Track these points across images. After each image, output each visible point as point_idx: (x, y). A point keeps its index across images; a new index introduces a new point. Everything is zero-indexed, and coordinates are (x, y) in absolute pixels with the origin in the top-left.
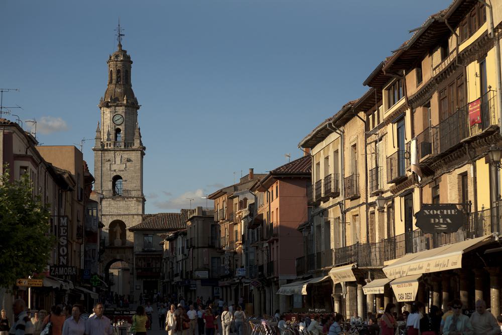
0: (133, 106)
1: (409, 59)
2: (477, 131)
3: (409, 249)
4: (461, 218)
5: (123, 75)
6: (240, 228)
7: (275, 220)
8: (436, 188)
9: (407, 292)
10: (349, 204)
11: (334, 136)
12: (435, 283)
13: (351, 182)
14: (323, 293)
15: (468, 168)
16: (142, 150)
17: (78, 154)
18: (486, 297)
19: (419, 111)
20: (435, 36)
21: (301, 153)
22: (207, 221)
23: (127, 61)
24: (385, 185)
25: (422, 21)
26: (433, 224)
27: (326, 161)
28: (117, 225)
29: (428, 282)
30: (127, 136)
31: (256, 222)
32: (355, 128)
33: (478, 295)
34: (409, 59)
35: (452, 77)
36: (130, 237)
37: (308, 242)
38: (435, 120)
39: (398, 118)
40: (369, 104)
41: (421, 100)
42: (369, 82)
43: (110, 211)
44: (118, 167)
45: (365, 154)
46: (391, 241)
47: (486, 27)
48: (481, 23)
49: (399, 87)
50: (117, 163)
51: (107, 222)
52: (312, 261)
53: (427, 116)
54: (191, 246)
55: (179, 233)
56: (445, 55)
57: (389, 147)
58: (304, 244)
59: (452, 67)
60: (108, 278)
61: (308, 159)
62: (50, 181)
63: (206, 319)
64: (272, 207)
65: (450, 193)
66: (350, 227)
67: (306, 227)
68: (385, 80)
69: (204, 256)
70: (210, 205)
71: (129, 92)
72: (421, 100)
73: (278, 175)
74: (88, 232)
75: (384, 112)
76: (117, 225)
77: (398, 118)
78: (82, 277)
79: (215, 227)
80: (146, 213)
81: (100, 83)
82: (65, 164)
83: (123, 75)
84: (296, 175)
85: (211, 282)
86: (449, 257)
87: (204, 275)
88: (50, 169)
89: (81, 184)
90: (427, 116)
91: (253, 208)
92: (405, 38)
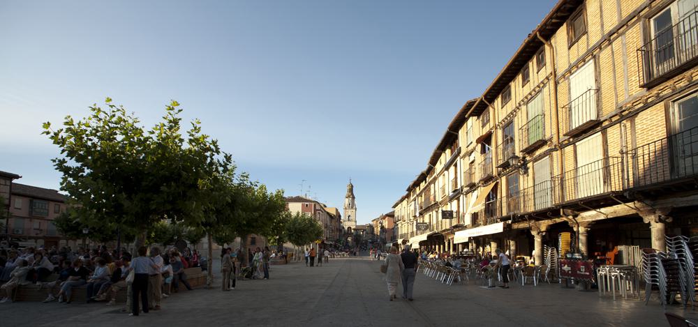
0: (354, 198)
1: (417, 184)
2: (433, 203)
3: (417, 235)
4: (428, 227)
5: (351, 190)
6: (379, 229)
7: (387, 227)
8: (423, 218)
9: (416, 246)
10: (403, 223)
11: (400, 205)
12: (189, 227)
13: (403, 217)
14: (396, 245)
15: (431, 213)
16: (356, 209)
17: (337, 210)
18: (435, 247)
19: (420, 198)
20: (423, 177)
21: (392, 210)
22: (371, 227)
23: (352, 186)
24: (412, 218)
25: (419, 173)
26: (421, 227)
27: (399, 212)
28: (349, 228)
29: (421, 243)
30: (352, 206)
31: (382, 227)
32: (405, 202)
33: (433, 247)
34: (417, 184)
35: (427, 188)
36: (353, 231)
37: (394, 232)
38: (423, 200)
39: (415, 200)
40: (408, 196)
41: (420, 195)
42: (407, 190)
43: (346, 225)
44: (350, 213)
45: (407, 210)
46: (412, 232)
47: (435, 174)
48: (666, 153)
49: (415, 192)
50: (350, 212)
51: (346, 228)
52: (394, 238)
53: (421, 199)
54: (367, 233)
55: (364, 230)
56: (426, 182)
57: (412, 208)
58: (392, 234)
59: (427, 186)
60: (347, 242)
61: (394, 212)
62: (328, 217)
63: (155, 232)
64: (386, 224)
65: (427, 220)
66: (404, 229)
67: (393, 229)
68: (411, 189)
69: (370, 236)
70: (371, 223)
71: (352, 194)
72: (420, 195)
73: (387, 215)
74: (340, 229)
75: (412, 198)
76: (349, 228)
77: (415, 200)
78: (338, 241)
79: (373, 229)
80: (28, 216)
81: (346, 193)
82: (333, 212)
83: (351, 190)
84: (391, 215)
85: (372, 243)
86: (424, 237)
87: (370, 241)
88: (328, 213)
89: (338, 217)
90: (421, 199)
91: (382, 224)
92: (415, 178)
